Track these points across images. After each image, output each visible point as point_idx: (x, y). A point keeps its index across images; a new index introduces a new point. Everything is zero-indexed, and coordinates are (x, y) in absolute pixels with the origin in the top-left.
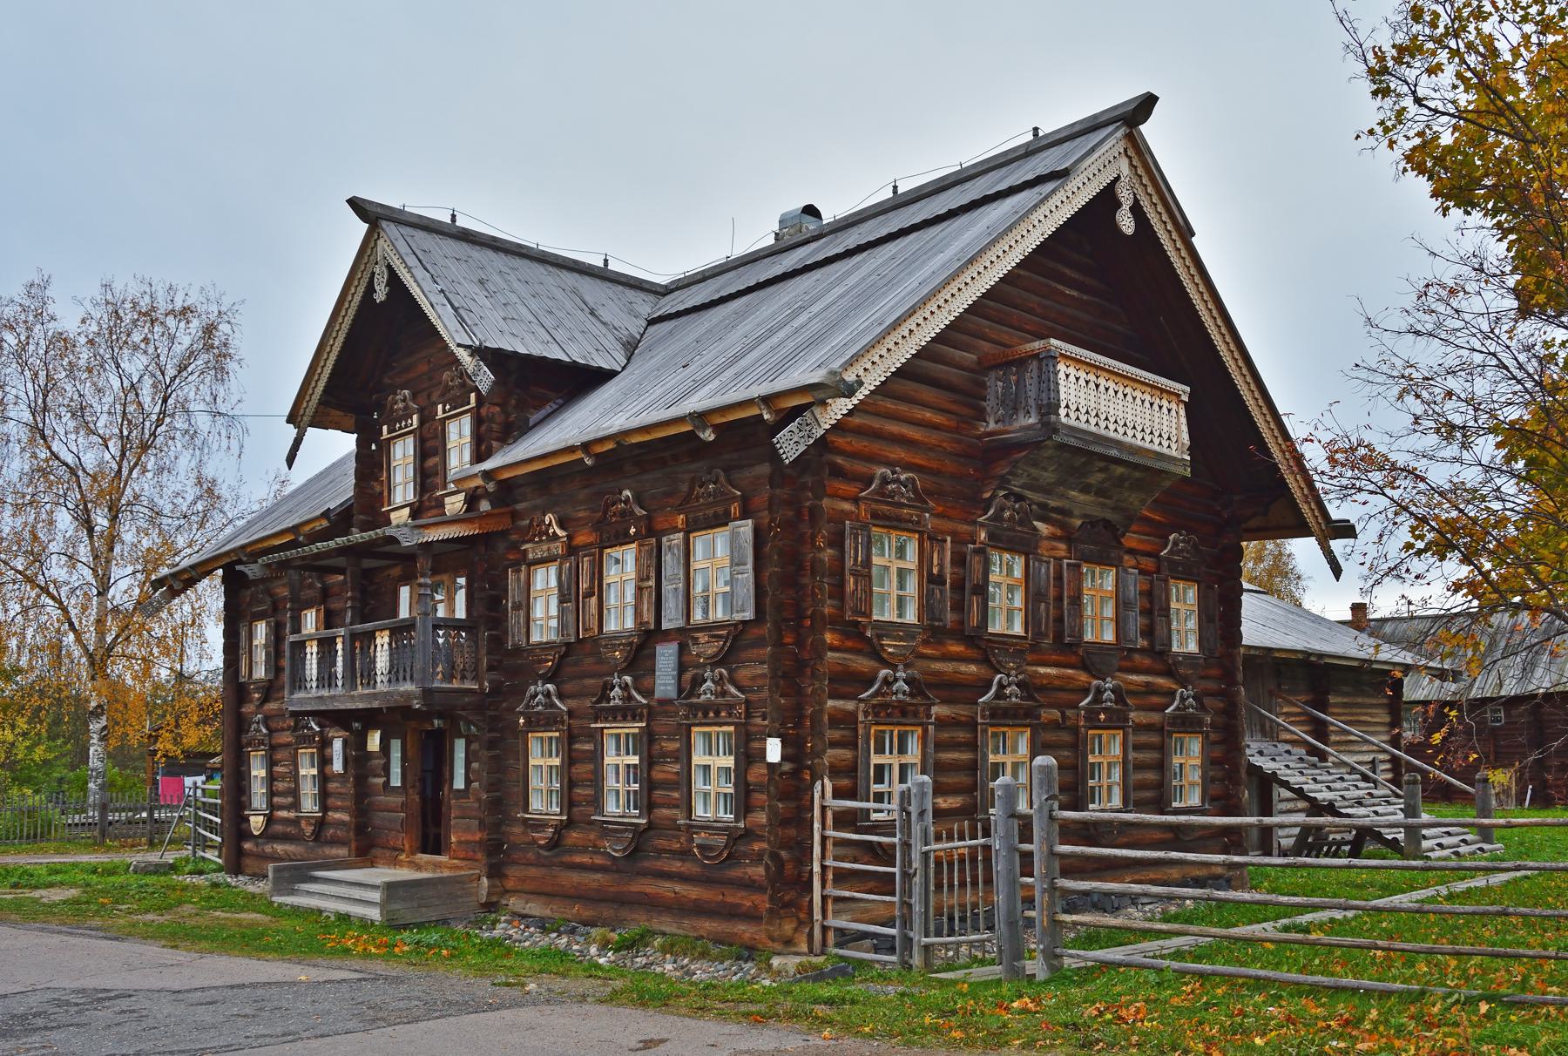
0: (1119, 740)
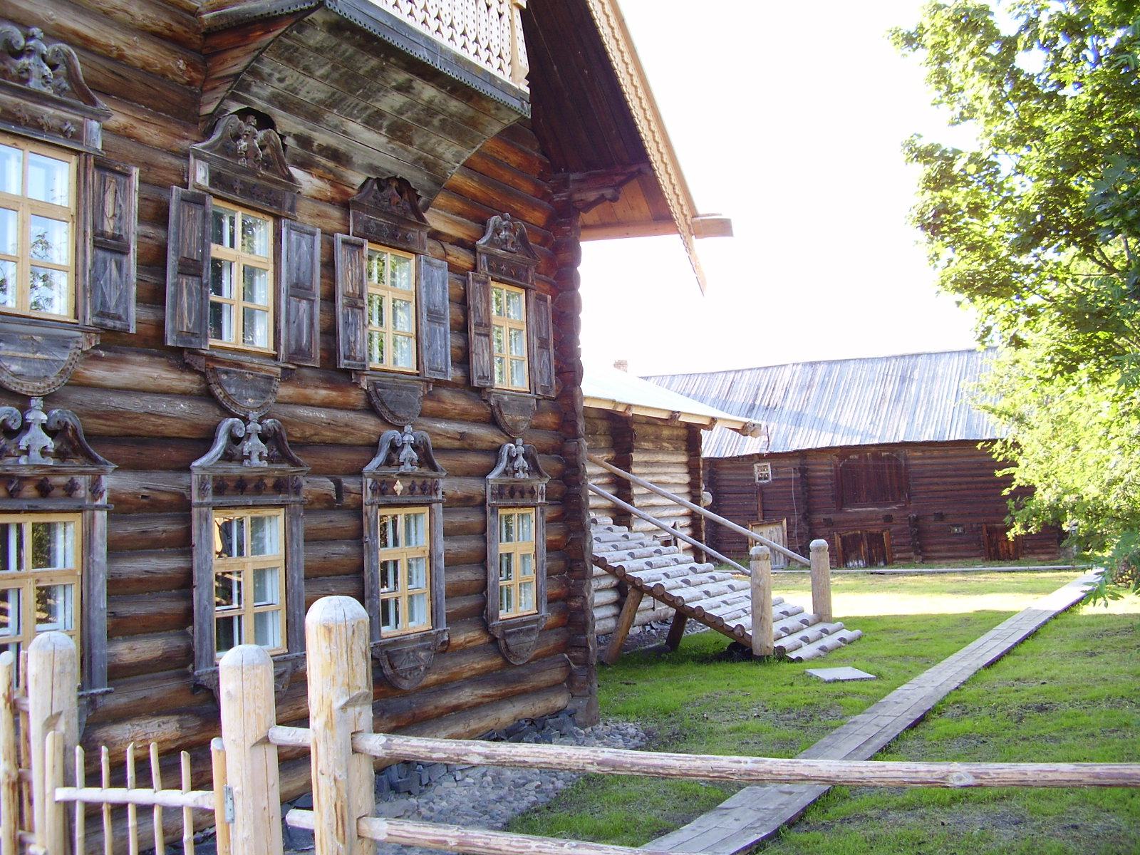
0: (424, 522)
